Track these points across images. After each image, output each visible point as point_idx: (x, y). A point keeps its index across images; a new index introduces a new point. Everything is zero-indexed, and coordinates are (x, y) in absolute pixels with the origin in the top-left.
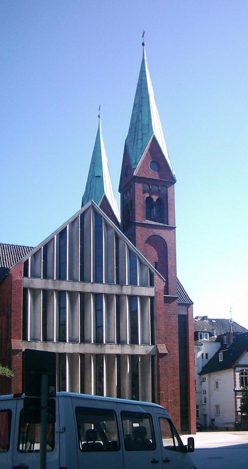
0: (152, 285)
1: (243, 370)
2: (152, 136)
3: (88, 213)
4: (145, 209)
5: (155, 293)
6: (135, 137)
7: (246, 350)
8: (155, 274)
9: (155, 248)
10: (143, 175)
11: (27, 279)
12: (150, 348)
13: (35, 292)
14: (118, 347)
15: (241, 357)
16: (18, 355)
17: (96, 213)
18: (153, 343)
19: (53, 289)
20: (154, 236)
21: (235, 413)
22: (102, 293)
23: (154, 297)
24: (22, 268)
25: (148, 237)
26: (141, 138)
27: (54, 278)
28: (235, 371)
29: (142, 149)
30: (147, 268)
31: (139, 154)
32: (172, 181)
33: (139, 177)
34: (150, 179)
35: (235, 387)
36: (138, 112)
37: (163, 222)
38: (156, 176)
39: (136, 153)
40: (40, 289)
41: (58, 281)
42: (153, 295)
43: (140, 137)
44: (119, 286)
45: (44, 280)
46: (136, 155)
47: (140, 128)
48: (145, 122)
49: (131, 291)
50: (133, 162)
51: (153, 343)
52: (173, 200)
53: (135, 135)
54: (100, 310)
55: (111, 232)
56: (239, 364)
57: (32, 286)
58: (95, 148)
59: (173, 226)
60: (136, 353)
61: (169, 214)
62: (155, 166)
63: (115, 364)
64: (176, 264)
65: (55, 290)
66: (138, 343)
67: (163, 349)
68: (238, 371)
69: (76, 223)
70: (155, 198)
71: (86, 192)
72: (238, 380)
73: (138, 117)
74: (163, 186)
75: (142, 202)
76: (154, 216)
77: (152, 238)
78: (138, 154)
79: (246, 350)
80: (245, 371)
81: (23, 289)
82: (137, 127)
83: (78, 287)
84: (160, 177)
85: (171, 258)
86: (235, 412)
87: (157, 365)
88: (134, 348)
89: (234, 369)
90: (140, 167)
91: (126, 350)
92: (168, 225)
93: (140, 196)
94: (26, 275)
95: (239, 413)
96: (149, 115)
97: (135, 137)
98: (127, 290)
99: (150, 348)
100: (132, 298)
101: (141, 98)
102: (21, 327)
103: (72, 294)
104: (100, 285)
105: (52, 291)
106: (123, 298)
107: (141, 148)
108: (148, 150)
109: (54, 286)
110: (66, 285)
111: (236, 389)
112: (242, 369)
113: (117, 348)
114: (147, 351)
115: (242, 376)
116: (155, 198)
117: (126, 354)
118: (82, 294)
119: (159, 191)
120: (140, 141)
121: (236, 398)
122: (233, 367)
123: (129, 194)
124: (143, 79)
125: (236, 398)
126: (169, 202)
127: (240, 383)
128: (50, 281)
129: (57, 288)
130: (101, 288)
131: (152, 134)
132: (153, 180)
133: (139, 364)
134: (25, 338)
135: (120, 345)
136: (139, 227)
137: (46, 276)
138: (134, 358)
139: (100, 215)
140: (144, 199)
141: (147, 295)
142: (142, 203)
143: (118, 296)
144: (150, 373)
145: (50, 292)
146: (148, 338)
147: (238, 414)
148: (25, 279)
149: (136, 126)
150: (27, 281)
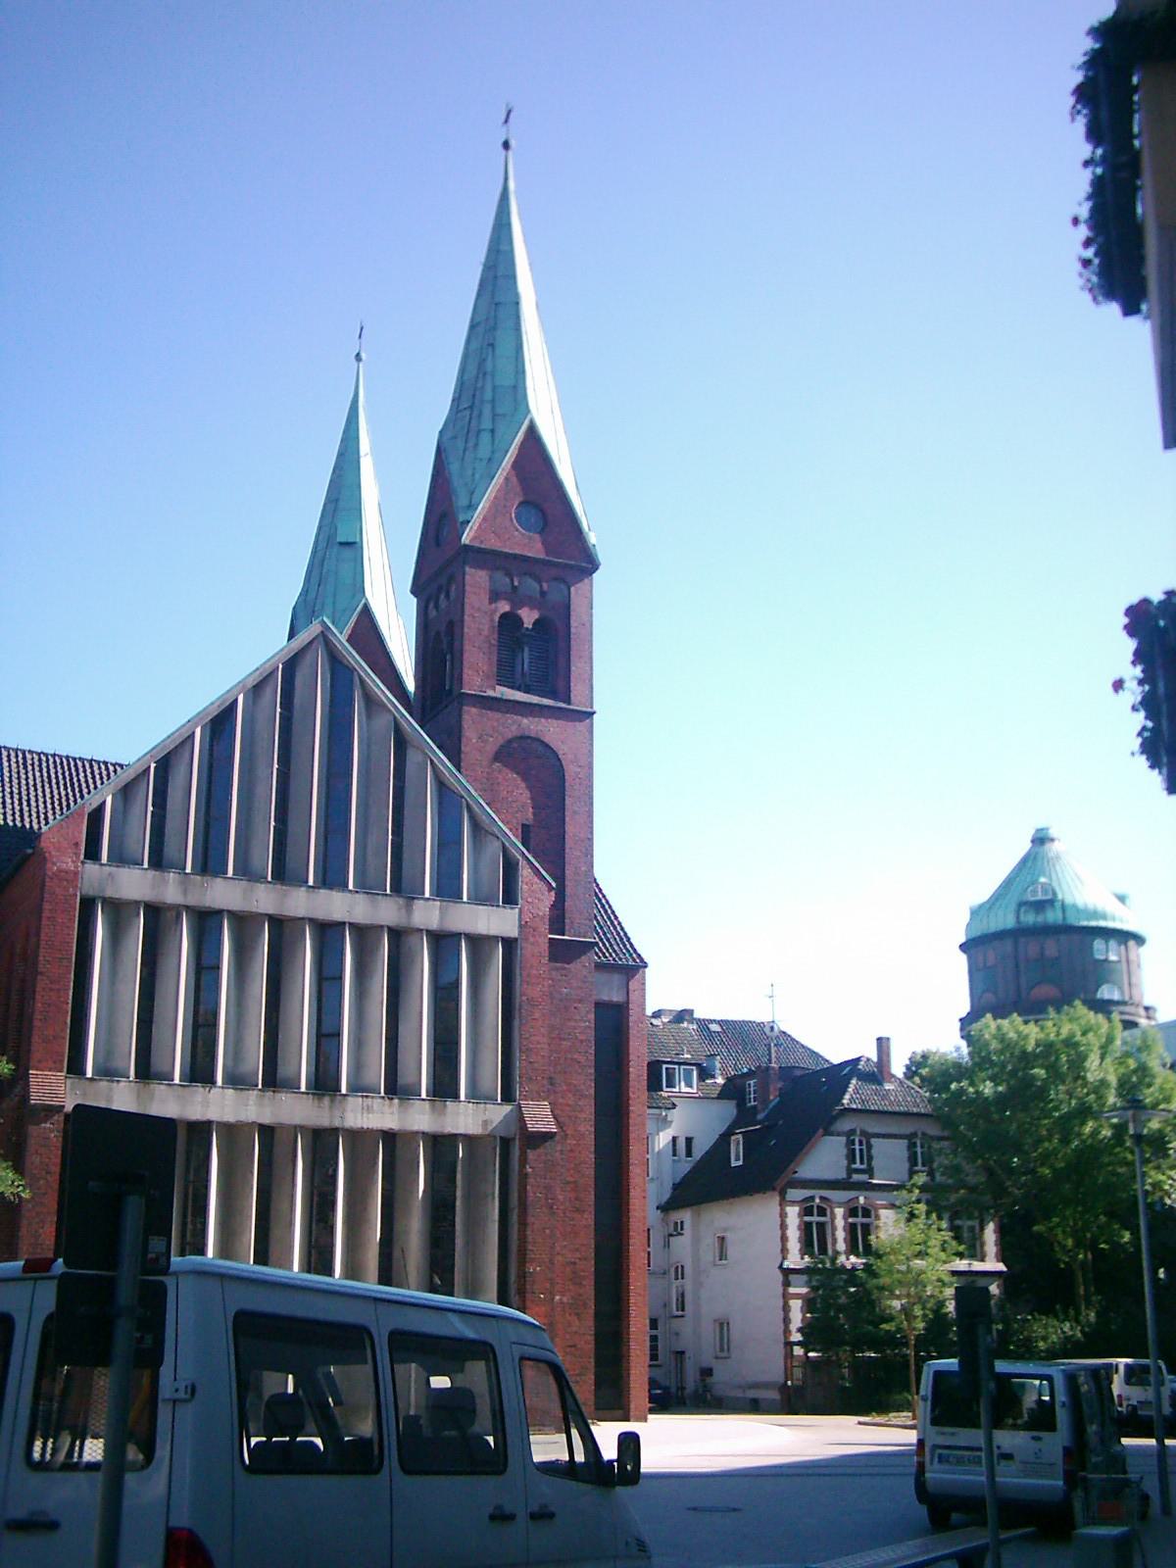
0: (510, 899)
1: (812, 1198)
2: (526, 423)
5: (520, 926)
7: (821, 1131)
8: (522, 862)
9: (525, 779)
10: (492, 543)
11: (97, 867)
12: (497, 1113)
13: (119, 911)
14: (391, 1105)
16: (48, 1125)
18: (508, 1096)
20: (523, 738)
22: (344, 923)
23: (516, 939)
25: (501, 741)
26: (491, 427)
28: (783, 1203)
29: (493, 462)
30: (497, 844)
31: (481, 477)
32: (587, 564)
33: (480, 551)
34: (515, 557)
35: (784, 1258)
36: (482, 348)
37: (553, 695)
38: (529, 544)
42: (514, 933)
43: (486, 424)
44: (401, 901)
47: (488, 395)
48: (505, 379)
50: (462, 500)
51: (508, 1096)
52: (588, 626)
54: (334, 979)
55: (382, 722)
56: (796, 1175)
57: (109, 893)
58: (341, 455)
59: (584, 709)
60: (449, 1129)
61: (573, 668)
65: (187, 908)
66: (456, 1096)
67: (540, 1117)
68: (793, 1203)
70: (529, 617)
71: (305, 592)
72: (794, 1234)
77: (515, 745)
78: (477, 476)
79: (821, 1131)
80: (817, 1200)
82: (477, 393)
83: (264, 899)
85: (575, 812)
86: (782, 1346)
88: (442, 1112)
90: (484, 519)
91: (417, 1116)
92: (569, 704)
93: (479, 609)
94: (93, 854)
95: (798, 1351)
98: (428, 914)
100: (443, 942)
101: (493, 306)
105: (177, 910)
107: (490, 460)
110: (224, 893)
112: (807, 1193)
114: (485, 1123)
115: (807, 1219)
116: (529, 617)
117: (417, 1133)
119: (543, 593)
120: (485, 438)
121: (786, 1297)
125: (786, 1297)
128: (172, 876)
129: (192, 900)
130: (341, 906)
133: (459, 1168)
134: (76, 1067)
135: (396, 1101)
136: (474, 710)
137: (158, 862)
138: (440, 1145)
139: (347, 667)
140: (492, 620)
141: (493, 932)
142: (486, 633)
143: (397, 935)
144: (494, 1198)
145: (170, 915)
147: (795, 1353)
148: (91, 868)
150: (94, 876)
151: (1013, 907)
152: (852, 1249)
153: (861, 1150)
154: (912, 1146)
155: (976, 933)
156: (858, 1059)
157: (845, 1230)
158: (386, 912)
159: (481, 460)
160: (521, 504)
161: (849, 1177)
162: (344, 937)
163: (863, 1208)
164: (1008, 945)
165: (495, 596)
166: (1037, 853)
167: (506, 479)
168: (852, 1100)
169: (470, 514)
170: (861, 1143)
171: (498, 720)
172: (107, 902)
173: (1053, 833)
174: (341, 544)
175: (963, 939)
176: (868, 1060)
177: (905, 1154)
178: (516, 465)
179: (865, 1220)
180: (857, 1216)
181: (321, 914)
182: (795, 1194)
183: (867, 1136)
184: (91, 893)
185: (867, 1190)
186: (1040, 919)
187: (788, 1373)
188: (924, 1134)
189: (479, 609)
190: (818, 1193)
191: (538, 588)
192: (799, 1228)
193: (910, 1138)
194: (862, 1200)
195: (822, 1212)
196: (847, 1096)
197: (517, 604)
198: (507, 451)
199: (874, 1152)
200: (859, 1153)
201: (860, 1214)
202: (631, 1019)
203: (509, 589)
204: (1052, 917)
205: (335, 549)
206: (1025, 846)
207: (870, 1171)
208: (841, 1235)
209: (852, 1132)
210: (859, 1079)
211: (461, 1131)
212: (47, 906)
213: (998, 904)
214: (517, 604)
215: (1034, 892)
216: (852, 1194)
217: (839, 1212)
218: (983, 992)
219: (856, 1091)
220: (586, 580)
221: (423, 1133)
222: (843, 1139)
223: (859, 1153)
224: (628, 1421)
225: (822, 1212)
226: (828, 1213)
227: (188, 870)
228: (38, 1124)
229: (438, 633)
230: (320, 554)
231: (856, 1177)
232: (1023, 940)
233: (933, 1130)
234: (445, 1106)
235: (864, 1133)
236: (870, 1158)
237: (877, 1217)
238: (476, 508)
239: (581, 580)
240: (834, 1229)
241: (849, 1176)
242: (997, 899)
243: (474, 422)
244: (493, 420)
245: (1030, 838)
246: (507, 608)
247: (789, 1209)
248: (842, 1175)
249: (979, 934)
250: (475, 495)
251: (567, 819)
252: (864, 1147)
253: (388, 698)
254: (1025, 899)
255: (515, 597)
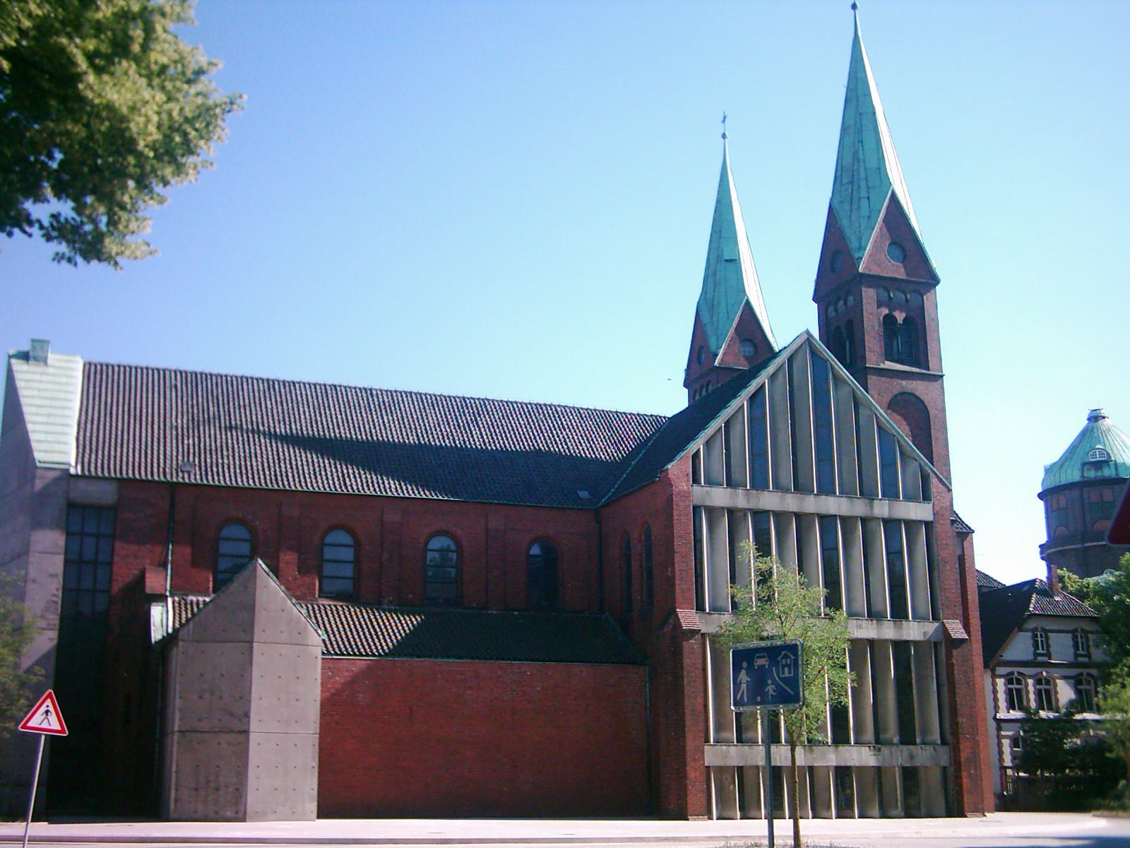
0: (926, 497)
1: (1012, 673)
2: (890, 192)
3: (800, 355)
4: (882, 338)
5: (934, 514)
6: (852, 193)
7: (1016, 629)
9: (905, 419)
10: (875, 271)
11: (699, 488)
12: (931, 627)
13: (711, 511)
15: (1007, 644)
17: (814, 353)
18: (935, 618)
19: (745, 509)
20: (903, 393)
21: (999, 773)
22: (836, 516)
23: (932, 522)
24: (689, 467)
25: (890, 397)
26: (866, 195)
27: (746, 486)
28: (994, 676)
29: (871, 218)
30: (916, 464)
33: (869, 276)
35: (997, 712)
36: (854, 144)
39: (860, 227)
40: (723, 508)
41: (754, 492)
42: (931, 518)
43: (864, 194)
44: (867, 501)
45: (729, 490)
46: (860, 232)
47: (862, 175)
48: (872, 164)
49: (890, 511)
50: (854, 244)
51: (935, 618)
52: (936, 320)
53: (852, 190)
55: (845, 391)
56: (1002, 658)
57: (708, 503)
58: (719, 201)
59: (937, 373)
60: (905, 638)
61: (929, 347)
62: (897, 252)
63: (866, 658)
64: (948, 452)
65: (750, 509)
66: (907, 618)
67: (956, 629)
68: (1000, 676)
69: (780, 376)
70: (900, 317)
72: (1002, 697)
73: (855, 153)
74: (914, 291)
75: (877, 325)
76: (898, 352)
77: (899, 398)
79: (1016, 629)
81: (693, 507)
82: (855, 174)
83: (791, 503)
84: (908, 275)
86: (998, 769)
87: (947, 662)
88: (900, 628)
89: (993, 671)
90: (870, 256)
91: (887, 630)
92: (929, 370)
93: (872, 314)
94: (696, 480)
95: (1009, 772)
96: (878, 150)
97: (852, 193)
98: (882, 509)
99: (931, 627)
100: (891, 524)
101: (858, 116)
102: (692, 585)
103: (781, 517)
104: (831, 499)
105: (744, 511)
106: (873, 525)
107: (869, 217)
108: (883, 221)
109: (749, 502)
110: (769, 500)
111: (998, 716)
112: (1009, 670)
113: (870, 626)
114: (925, 634)
116: (900, 317)
117: (887, 640)
118: (799, 516)
119: (907, 300)
120: (864, 203)
121: (999, 737)
122: (991, 667)
123: (844, 308)
124: (859, 75)
125: (999, 737)
126: (927, 324)
127: (1006, 701)
128: (740, 491)
129: (752, 505)
130: (834, 505)
131: (889, 189)
132: (896, 279)
133: (912, 661)
134: (700, 608)
135: (874, 622)
136: (874, 377)
137: (730, 484)
139: (822, 359)
140: (879, 319)
141: (919, 518)
143: (865, 521)
144: (932, 678)
146: (925, 607)
147: (1008, 773)
148: (696, 488)
149: (853, 171)
150: (699, 493)
151: (1079, 466)
152: (1011, 706)
153: (1042, 641)
154: (1075, 638)
155: (1052, 483)
156: (1034, 581)
157: (1034, 693)
158: (858, 508)
159: (864, 217)
160: (890, 245)
161: (1036, 659)
162: (769, 521)
163: (1045, 679)
164: (1075, 493)
165: (880, 305)
166: (1092, 428)
167: (881, 229)
168: (1035, 608)
169: (861, 253)
170: (1041, 636)
171: (888, 383)
172: (705, 507)
173: (1104, 413)
174: (726, 260)
175: (1040, 490)
176: (1041, 581)
177: (1071, 643)
178: (884, 221)
179: (1047, 687)
180: (1042, 684)
181: (823, 511)
182: (1001, 670)
183: (1046, 631)
184: (699, 503)
185: (1046, 667)
186: (1099, 474)
187: (1004, 787)
188: (1082, 630)
189: (872, 314)
190: (1016, 670)
191: (904, 298)
192: (1005, 692)
193: (1074, 632)
194: (1044, 674)
195: (1019, 682)
196: (1032, 606)
197: (892, 309)
198: (880, 211)
199: (1050, 642)
200: (1041, 642)
201: (1084, 683)
202: (966, 565)
203: (887, 298)
204: (1108, 472)
205: (723, 264)
206: (1084, 423)
207: (1049, 656)
208: (1032, 696)
209: (1036, 629)
210: (1037, 594)
211: (911, 639)
212: (675, 513)
213: (1067, 464)
214: (892, 309)
215: (1094, 455)
216: (1039, 670)
217: (1030, 681)
218: (1058, 527)
219: (1037, 602)
220: (932, 291)
221: (891, 640)
222: (1030, 634)
223: (1041, 642)
224: (962, 814)
225: (1019, 682)
226: (1023, 682)
227: (748, 488)
228: (687, 640)
229: (838, 328)
230: (712, 268)
231: (1040, 659)
232: (1086, 489)
233: (1087, 626)
234: (902, 624)
235: (1043, 630)
236: (1048, 646)
237: (1055, 685)
238: (865, 250)
239: (929, 291)
240: (1028, 692)
241: (1076, 659)
242: (1065, 461)
243: (855, 192)
244: (868, 192)
245: (1087, 417)
246: (887, 312)
247: (998, 680)
248: (1030, 657)
249: (1053, 486)
250: (862, 242)
251: (933, 443)
252: (1044, 639)
253: (851, 381)
254: (1086, 461)
255: (889, 303)
